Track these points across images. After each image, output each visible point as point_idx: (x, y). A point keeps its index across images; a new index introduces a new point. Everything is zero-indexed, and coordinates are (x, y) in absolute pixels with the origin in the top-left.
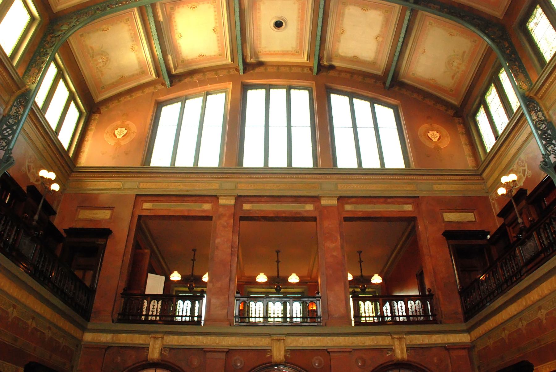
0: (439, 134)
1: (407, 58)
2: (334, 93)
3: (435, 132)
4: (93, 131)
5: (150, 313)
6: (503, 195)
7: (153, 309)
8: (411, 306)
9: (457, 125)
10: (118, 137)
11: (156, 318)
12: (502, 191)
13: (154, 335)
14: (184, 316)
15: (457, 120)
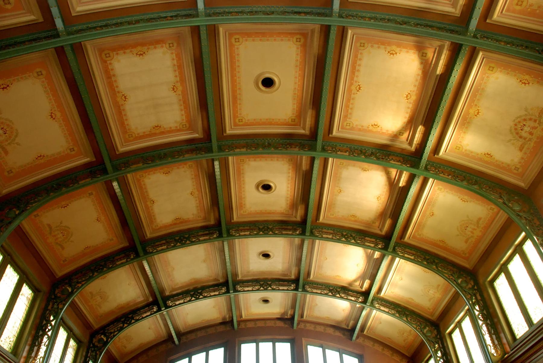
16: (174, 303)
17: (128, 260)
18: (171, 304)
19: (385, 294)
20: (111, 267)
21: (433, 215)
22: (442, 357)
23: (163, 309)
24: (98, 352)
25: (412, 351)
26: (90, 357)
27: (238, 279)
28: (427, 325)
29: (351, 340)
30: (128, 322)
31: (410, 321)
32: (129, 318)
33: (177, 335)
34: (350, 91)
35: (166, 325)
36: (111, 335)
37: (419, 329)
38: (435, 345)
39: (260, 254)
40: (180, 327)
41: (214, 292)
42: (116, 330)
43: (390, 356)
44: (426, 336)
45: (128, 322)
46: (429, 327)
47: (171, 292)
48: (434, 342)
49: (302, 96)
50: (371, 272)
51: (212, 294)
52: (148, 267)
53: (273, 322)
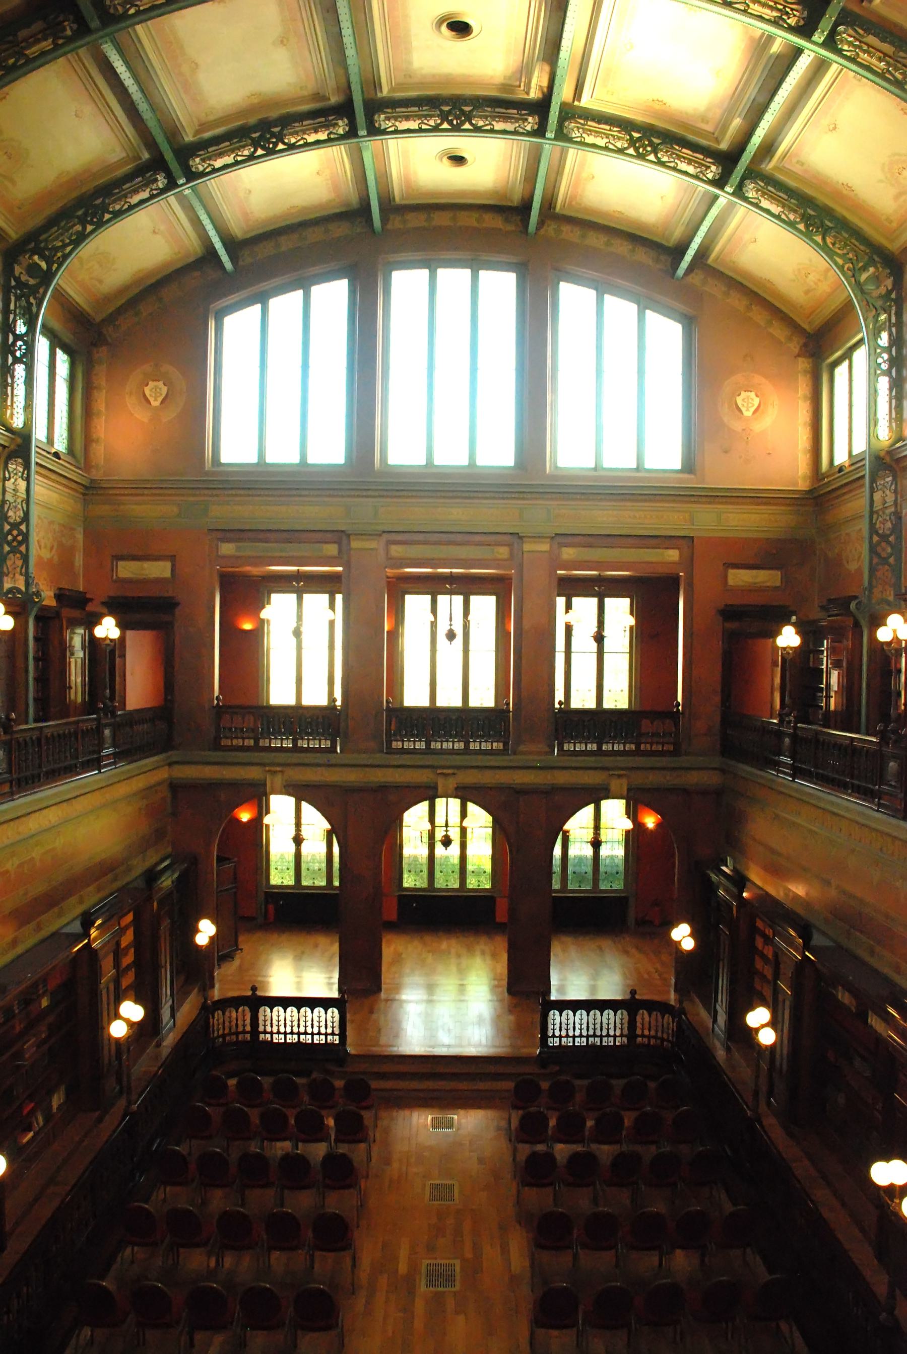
0: (150, 383)
4: (104, 391)
5: (639, 1032)
7: (594, 1025)
8: (333, 1017)
9: (799, 375)
10: (155, 403)
11: (237, 1037)
14: (591, 1036)
15: (803, 364)
16: (210, 165)
17: (60, 42)
18: (201, 168)
20: (14, 64)
22: (888, 350)
23: (181, 182)
24: (32, 300)
25: (818, 322)
26: (15, 311)
27: (379, 95)
28: (871, 262)
29: (673, 278)
30: (95, 220)
31: (831, 246)
32: (96, 206)
33: (225, 245)
35: (196, 222)
36: (55, 255)
37: (848, 269)
38: (878, 315)
39: (440, 22)
40: (236, 230)
41: (316, 132)
42: (68, 241)
43: (762, 324)
44: (862, 291)
45: (95, 220)
46: (876, 268)
47: (197, 132)
48: (879, 309)
50: (752, 98)
51: (311, 138)
52: (121, 62)
53: (475, 215)
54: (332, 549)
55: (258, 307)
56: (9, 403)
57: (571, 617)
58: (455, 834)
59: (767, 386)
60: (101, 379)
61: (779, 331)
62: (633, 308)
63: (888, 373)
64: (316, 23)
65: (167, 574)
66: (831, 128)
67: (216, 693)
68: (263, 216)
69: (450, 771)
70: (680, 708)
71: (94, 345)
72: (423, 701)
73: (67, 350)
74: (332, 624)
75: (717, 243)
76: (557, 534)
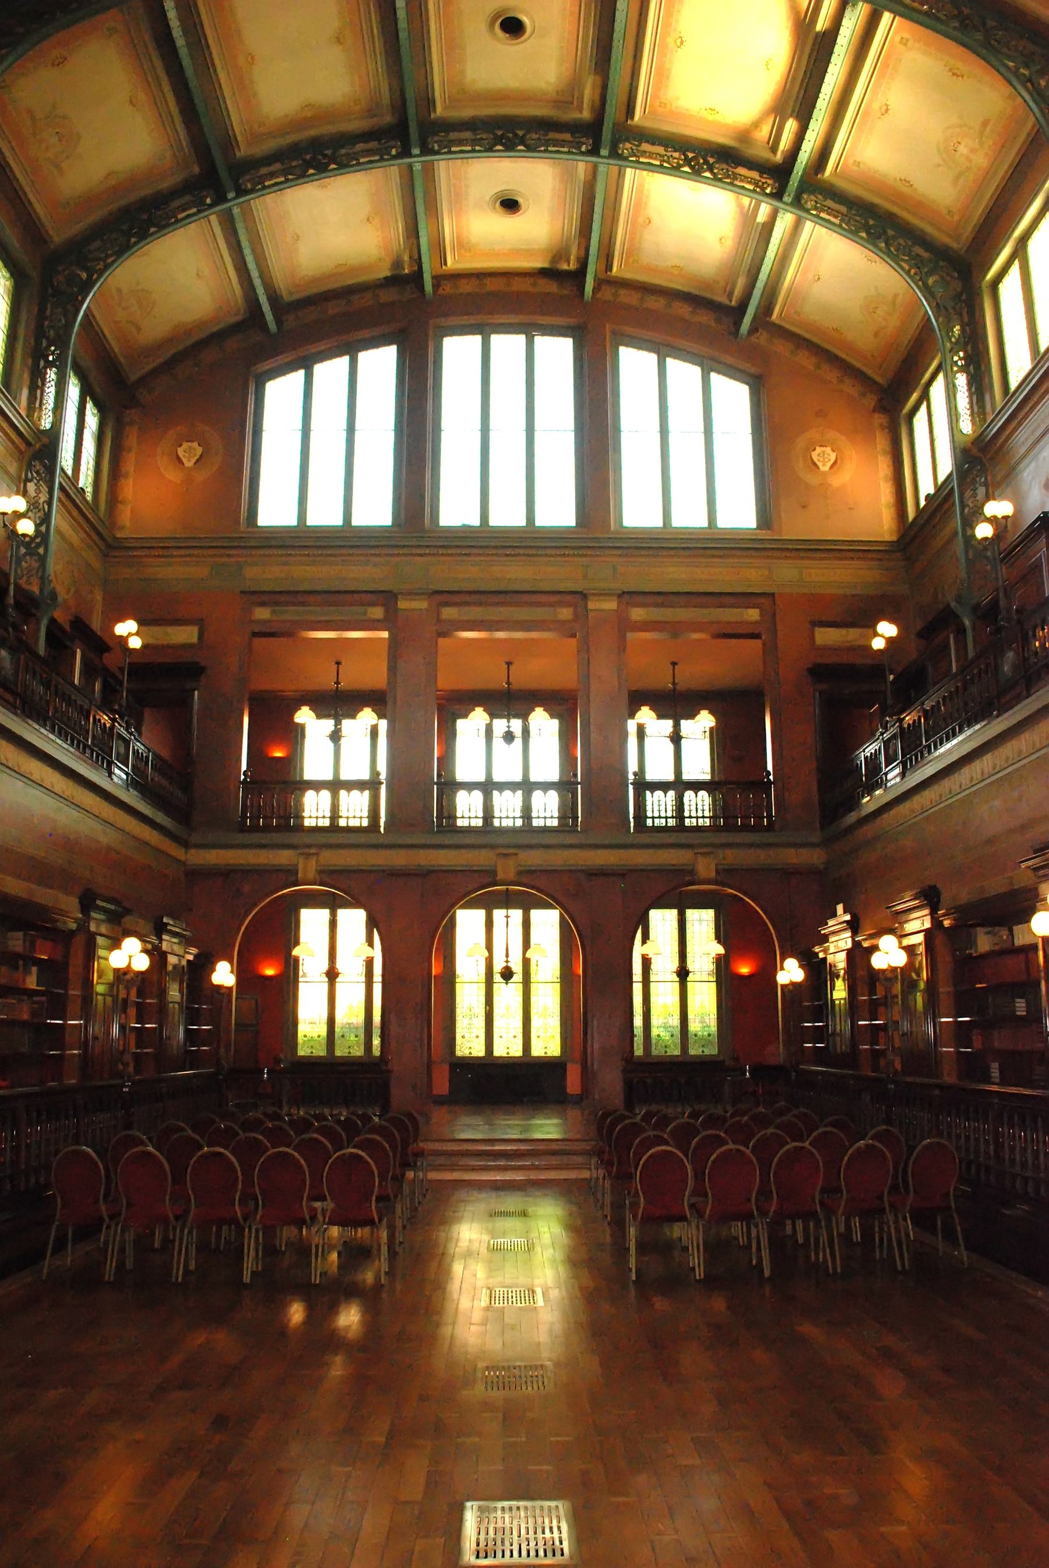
1: (566, 853)
2: (627, 345)
3: (828, 450)
6: (985, 539)
9: (877, 432)
10: (189, 464)
12: (984, 531)
13: (306, 850)
15: (879, 419)
19: (836, 170)
21: (887, 110)
34: (664, 46)
43: (835, 381)
49: (563, 229)
53: (529, 281)
54: (377, 612)
55: (301, 374)
56: (37, 405)
57: (648, 949)
58: (517, 967)
59: (842, 440)
60: (132, 438)
61: (850, 388)
62: (696, 371)
63: (963, 369)
64: (373, 14)
65: (195, 639)
66: (883, 111)
67: (244, 767)
68: (311, 273)
69: (511, 851)
70: (771, 777)
71: (126, 407)
72: (478, 1050)
73: (97, 404)
74: (369, 963)
75: (780, 293)
76: (624, 593)
